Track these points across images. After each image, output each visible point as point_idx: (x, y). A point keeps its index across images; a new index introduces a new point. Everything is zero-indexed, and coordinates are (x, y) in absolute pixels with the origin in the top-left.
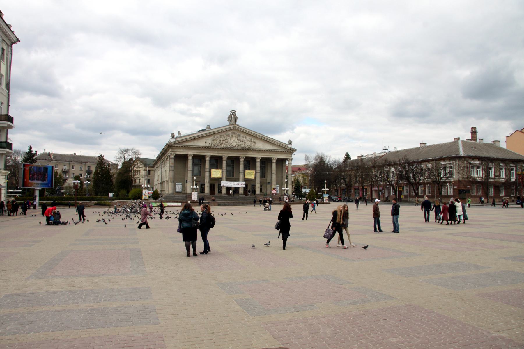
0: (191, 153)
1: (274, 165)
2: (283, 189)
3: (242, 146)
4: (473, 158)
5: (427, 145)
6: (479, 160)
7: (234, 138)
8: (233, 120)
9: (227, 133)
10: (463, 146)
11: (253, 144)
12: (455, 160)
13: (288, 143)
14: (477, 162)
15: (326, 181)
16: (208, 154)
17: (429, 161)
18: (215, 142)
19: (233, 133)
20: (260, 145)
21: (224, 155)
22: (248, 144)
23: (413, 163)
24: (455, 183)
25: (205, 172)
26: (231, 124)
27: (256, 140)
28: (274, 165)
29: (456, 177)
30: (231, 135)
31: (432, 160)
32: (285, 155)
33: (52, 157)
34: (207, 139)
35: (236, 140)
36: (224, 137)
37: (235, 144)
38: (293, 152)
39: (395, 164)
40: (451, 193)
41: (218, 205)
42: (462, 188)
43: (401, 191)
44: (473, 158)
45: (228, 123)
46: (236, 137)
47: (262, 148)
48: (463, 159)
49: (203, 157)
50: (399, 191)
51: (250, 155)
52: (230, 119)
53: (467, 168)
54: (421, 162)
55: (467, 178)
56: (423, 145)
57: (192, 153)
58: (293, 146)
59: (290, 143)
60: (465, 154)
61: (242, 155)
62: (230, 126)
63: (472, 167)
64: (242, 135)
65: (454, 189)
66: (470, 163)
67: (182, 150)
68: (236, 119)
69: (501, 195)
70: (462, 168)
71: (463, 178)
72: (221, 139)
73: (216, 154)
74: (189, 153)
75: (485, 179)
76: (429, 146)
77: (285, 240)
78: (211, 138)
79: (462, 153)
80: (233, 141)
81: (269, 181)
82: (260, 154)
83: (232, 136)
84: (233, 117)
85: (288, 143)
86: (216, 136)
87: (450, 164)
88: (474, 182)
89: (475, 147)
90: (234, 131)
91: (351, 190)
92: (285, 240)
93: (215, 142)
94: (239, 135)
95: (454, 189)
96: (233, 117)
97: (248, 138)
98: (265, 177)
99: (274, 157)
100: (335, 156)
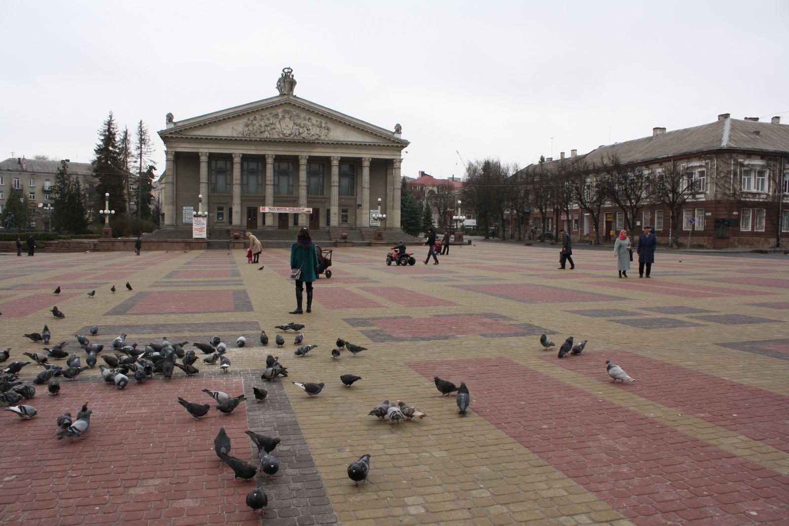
0: (204, 150)
1: (366, 172)
2: (454, 217)
3: (303, 135)
4: (749, 153)
5: (667, 131)
6: (762, 158)
7: (287, 120)
8: (287, 87)
9: (274, 112)
10: (732, 129)
11: (324, 132)
12: (711, 159)
13: (394, 130)
14: (758, 162)
15: (107, 194)
16: (237, 151)
17: (660, 161)
18: (251, 128)
19: (285, 111)
20: (338, 134)
21: (269, 153)
22: (315, 131)
23: (632, 166)
24: (704, 206)
25: (362, 188)
26: (282, 95)
27: (330, 125)
28: (366, 172)
29: (708, 192)
30: (280, 116)
31: (668, 159)
32: (387, 152)
33: (24, 166)
34: (235, 122)
35: (291, 125)
36: (268, 119)
37: (289, 132)
38: (403, 147)
39: (596, 171)
40: (699, 226)
41: (353, 246)
42: (723, 215)
43: (611, 222)
44: (749, 153)
45: (277, 93)
46: (290, 118)
47: (342, 139)
48: (727, 156)
49: (261, 159)
50: (607, 222)
51: (319, 152)
52: (282, 84)
53: (735, 174)
54: (647, 163)
55: (734, 194)
56: (659, 132)
57: (207, 151)
58: (403, 136)
59: (398, 129)
60: (733, 145)
61: (304, 154)
62: (280, 98)
63: (747, 173)
64: (303, 115)
65: (706, 217)
66: (742, 165)
67: (187, 145)
68: (293, 83)
69: (742, 230)
70: (722, 175)
71: (725, 194)
72: (263, 124)
73: (252, 151)
74: (201, 150)
75: (774, 197)
76: (670, 133)
77: (25, 365)
78: (244, 121)
79: (725, 143)
80: (286, 127)
81: (358, 203)
82: (339, 150)
83: (284, 117)
84: (287, 82)
85: (394, 130)
86: (252, 118)
87: (701, 166)
88: (742, 204)
89: (757, 133)
90: (287, 109)
91: (527, 220)
92: (25, 365)
93: (251, 128)
94: (298, 116)
95: (706, 217)
96: (287, 82)
97: (314, 120)
98: (353, 195)
99: (367, 155)
100: (517, 156)
